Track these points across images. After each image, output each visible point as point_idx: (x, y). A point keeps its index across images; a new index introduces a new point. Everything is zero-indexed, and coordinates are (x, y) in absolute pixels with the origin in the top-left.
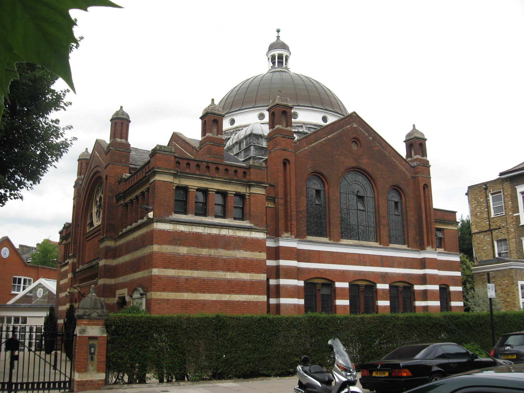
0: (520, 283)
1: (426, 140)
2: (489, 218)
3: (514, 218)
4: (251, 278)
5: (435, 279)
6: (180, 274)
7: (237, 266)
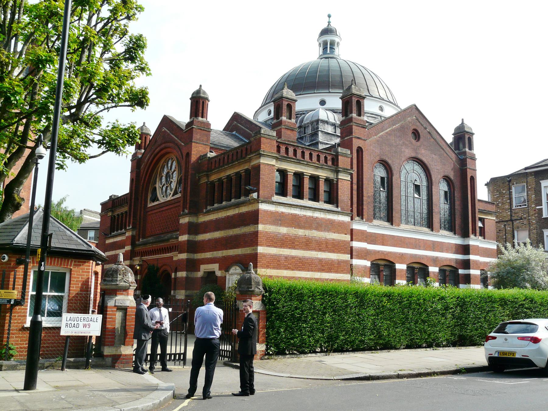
1: (473, 134)
2: (511, 209)
3: (537, 211)
5: (477, 264)
6: (281, 253)
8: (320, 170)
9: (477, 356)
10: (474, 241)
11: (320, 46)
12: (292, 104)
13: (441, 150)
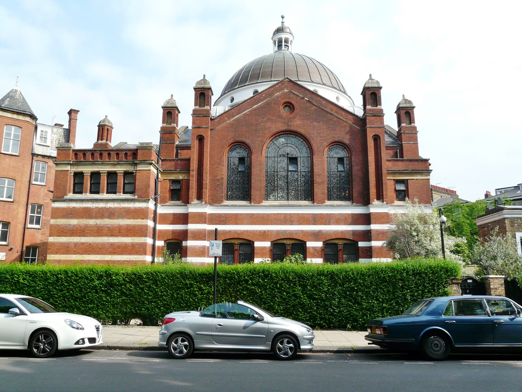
0: (519, 235)
4: (132, 241)
6: (71, 241)
7: (120, 232)
8: (119, 166)
9: (152, 336)
10: (376, 208)
11: (275, 44)
12: (377, 92)
13: (329, 115)
